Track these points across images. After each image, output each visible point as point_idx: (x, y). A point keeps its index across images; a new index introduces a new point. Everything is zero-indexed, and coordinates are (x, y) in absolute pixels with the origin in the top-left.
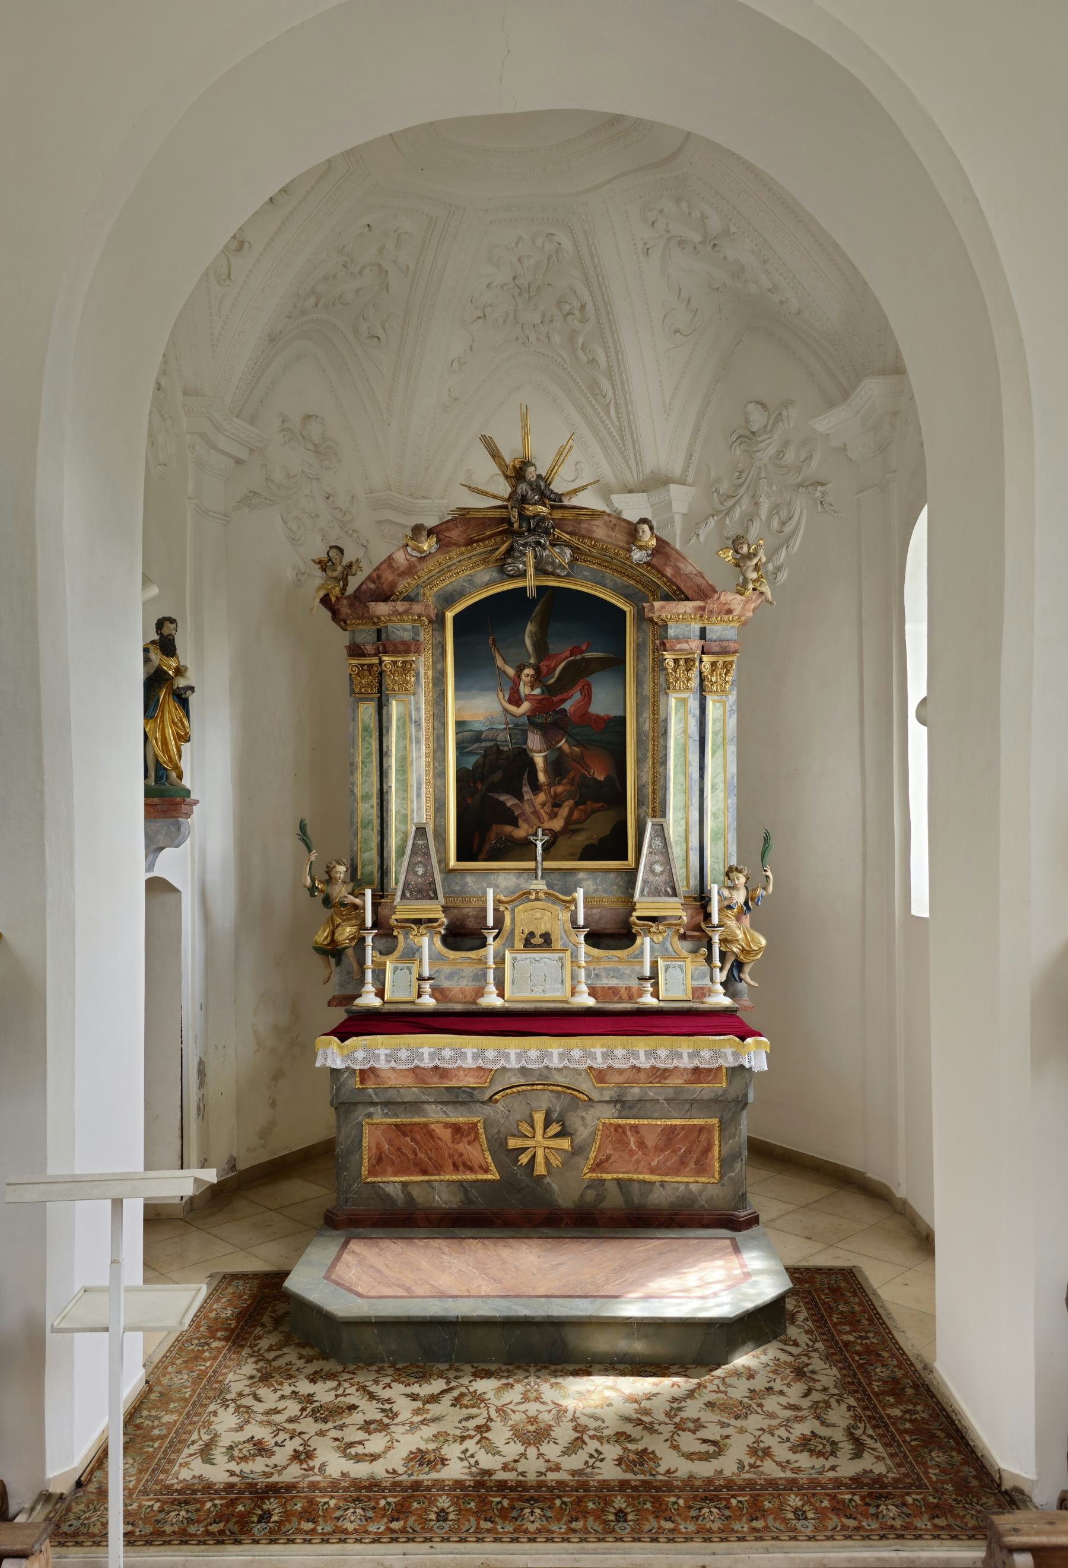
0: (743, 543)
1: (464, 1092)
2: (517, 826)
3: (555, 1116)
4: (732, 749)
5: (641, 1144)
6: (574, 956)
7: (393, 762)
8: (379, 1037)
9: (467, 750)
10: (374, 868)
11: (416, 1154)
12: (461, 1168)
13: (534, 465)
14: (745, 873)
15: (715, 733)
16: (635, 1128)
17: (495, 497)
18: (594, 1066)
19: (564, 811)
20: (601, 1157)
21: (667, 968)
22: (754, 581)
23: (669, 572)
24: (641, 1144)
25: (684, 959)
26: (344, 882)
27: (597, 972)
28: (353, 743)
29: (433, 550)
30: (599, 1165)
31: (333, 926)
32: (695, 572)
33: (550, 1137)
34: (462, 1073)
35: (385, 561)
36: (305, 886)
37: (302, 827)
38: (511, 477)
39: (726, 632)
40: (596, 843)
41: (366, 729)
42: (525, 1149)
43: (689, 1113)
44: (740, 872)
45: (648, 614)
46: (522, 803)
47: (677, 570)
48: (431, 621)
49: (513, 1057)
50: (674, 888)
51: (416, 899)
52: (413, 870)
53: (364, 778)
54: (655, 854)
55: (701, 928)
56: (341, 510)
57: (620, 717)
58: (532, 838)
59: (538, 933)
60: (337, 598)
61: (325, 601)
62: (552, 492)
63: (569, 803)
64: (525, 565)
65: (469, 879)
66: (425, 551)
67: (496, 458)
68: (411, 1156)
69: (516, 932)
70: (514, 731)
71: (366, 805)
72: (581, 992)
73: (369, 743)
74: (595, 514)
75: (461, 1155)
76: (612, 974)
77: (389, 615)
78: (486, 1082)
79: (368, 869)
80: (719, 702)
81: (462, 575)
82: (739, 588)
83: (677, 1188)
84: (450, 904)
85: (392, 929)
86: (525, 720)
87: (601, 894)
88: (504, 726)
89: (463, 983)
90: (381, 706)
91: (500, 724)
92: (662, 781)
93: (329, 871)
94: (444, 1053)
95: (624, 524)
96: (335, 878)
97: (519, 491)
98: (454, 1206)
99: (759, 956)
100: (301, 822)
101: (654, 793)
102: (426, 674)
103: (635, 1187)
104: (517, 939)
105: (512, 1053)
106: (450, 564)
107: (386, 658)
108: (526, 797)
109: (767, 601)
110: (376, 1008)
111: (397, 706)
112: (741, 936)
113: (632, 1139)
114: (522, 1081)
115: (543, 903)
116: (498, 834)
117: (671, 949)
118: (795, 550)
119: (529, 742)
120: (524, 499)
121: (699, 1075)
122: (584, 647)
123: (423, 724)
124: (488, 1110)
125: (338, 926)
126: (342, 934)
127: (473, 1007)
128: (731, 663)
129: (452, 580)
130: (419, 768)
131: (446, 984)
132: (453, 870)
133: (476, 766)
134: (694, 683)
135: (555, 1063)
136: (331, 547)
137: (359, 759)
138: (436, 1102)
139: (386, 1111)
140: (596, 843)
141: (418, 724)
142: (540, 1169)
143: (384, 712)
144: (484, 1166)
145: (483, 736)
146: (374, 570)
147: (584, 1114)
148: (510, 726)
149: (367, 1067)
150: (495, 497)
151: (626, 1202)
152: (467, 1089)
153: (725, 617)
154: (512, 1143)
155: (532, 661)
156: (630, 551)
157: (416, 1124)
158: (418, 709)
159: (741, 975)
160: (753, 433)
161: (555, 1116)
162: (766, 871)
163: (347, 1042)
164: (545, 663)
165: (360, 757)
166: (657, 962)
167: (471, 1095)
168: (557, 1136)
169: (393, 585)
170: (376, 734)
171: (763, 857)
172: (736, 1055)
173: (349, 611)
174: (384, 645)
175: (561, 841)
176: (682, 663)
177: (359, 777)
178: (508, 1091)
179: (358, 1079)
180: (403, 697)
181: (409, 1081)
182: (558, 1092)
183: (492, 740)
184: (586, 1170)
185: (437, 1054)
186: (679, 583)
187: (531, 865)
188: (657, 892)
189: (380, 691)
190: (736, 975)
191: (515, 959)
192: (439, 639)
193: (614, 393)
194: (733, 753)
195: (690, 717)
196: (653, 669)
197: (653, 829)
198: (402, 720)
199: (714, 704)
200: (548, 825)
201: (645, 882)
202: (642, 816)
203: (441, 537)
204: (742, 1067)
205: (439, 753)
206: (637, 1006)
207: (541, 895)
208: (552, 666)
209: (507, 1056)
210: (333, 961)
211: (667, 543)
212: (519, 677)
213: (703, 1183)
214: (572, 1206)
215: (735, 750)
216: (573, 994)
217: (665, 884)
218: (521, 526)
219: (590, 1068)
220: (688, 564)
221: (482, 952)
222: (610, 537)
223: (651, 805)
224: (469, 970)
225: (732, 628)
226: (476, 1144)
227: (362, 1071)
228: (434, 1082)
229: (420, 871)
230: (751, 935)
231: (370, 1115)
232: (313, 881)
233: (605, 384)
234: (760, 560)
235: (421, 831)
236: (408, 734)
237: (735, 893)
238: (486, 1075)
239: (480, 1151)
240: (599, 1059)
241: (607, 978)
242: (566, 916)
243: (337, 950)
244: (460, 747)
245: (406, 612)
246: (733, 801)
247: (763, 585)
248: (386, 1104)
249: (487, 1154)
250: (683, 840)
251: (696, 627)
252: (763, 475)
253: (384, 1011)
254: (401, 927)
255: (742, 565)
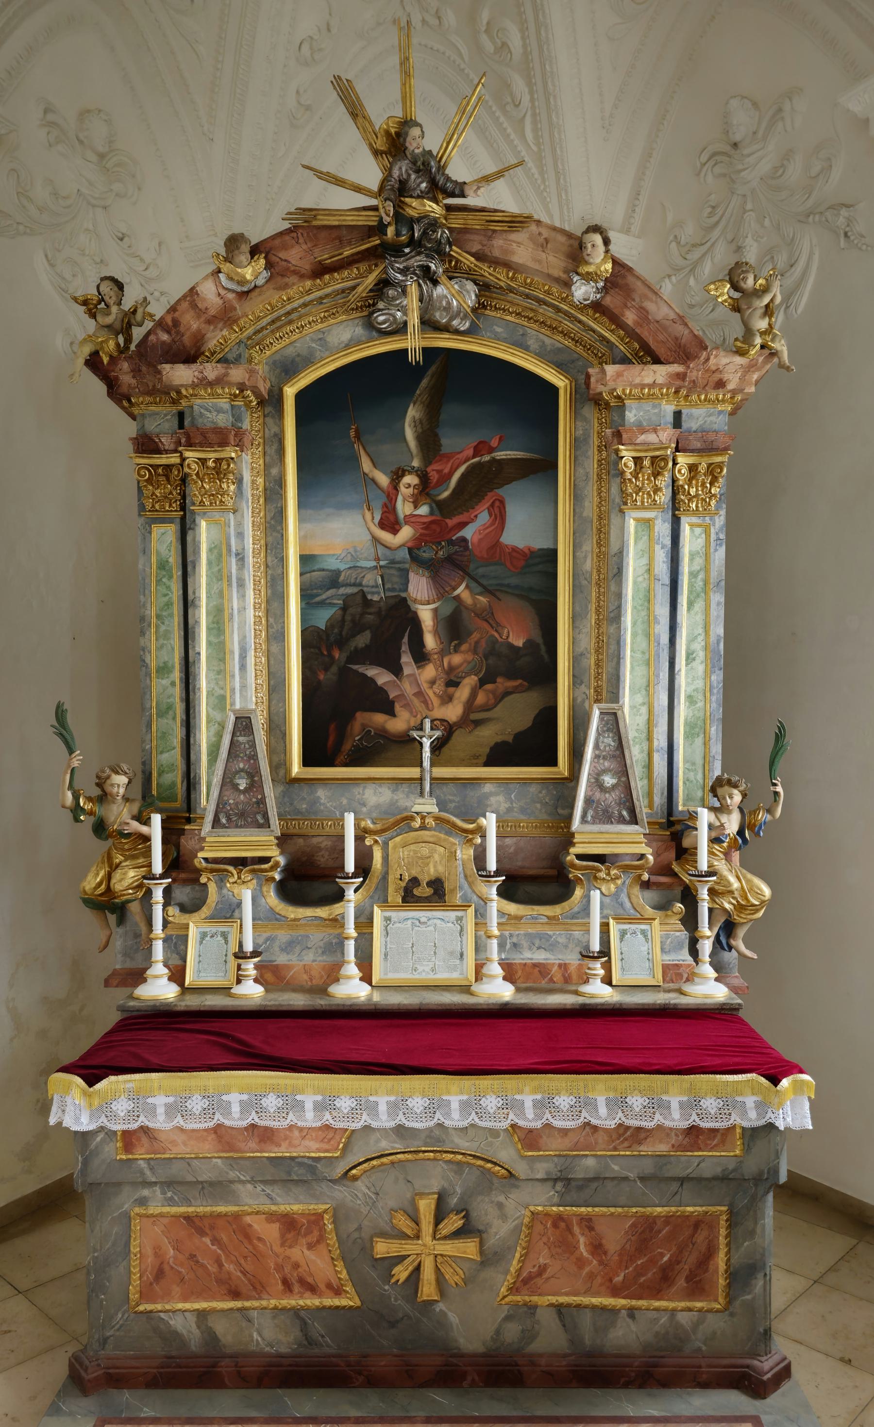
0: (747, 272)
1: (301, 1164)
2: (391, 713)
3: (453, 1201)
4: (718, 598)
5: (597, 1248)
6: (481, 915)
7: (202, 616)
8: (154, 1075)
9: (318, 599)
10: (177, 777)
11: (221, 1266)
12: (296, 1288)
13: (420, 126)
14: (742, 788)
15: (693, 575)
16: (588, 1223)
17: (358, 189)
18: (521, 1123)
19: (463, 693)
20: (529, 1269)
21: (623, 934)
22: (763, 333)
23: (630, 317)
24: (597, 1248)
25: (643, 919)
26: (126, 799)
27: (515, 940)
28: (144, 588)
29: (261, 281)
30: (525, 1282)
31: (110, 866)
32: (672, 316)
33: (445, 1238)
34: (296, 1133)
35: (184, 297)
36: (64, 807)
37: (60, 714)
38: (382, 153)
39: (713, 418)
40: (510, 741)
41: (163, 565)
42: (401, 1259)
43: (677, 1198)
44: (735, 786)
45: (596, 387)
46: (400, 680)
47: (643, 313)
48: (261, 403)
49: (383, 1108)
50: (632, 811)
51: (237, 827)
52: (231, 782)
53: (161, 641)
54: (604, 758)
55: (672, 870)
56: (142, 260)
57: (548, 550)
58: (415, 734)
59: (424, 879)
60: (111, 357)
61: (93, 362)
62: (448, 179)
63: (469, 683)
64: (405, 314)
65: (322, 793)
66: (248, 281)
67: (360, 119)
68: (213, 1268)
69: (391, 878)
70: (388, 571)
71: (165, 682)
72: (492, 977)
73: (168, 588)
74: (516, 222)
75: (296, 1266)
76: (537, 942)
77: (194, 386)
78: (337, 1149)
79: (168, 778)
80: (699, 526)
81: (307, 330)
82: (739, 344)
83: (656, 1320)
84: (292, 831)
85: (198, 872)
86: (404, 554)
87: (516, 815)
88: (374, 563)
89: (309, 957)
90: (185, 529)
91: (367, 559)
92: (613, 647)
93: (101, 783)
94: (265, 1102)
95: (562, 239)
96: (111, 795)
97: (396, 173)
98: (284, 1350)
99: (760, 914)
100: (58, 707)
101: (598, 665)
102: (253, 482)
103: (586, 1321)
104: (391, 889)
105: (383, 1102)
106: (289, 308)
107: (191, 455)
108: (407, 671)
109: (781, 366)
110: (168, 1004)
111: (208, 529)
112: (736, 885)
113: (582, 1240)
114: (399, 1147)
115: (433, 833)
116: (364, 726)
117: (628, 905)
118: (799, 311)
119: (411, 588)
120: (403, 189)
121: (697, 1137)
122: (494, 443)
123: (250, 560)
124: (341, 1193)
125: (118, 866)
126: (121, 880)
127: (320, 1002)
128: (720, 466)
129: (293, 338)
130: (242, 624)
131: (281, 959)
132: (297, 780)
133: (331, 624)
134: (664, 497)
135: (455, 1119)
136: (103, 279)
137: (152, 612)
138: (253, 1181)
139: (169, 1194)
140: (510, 741)
141: (241, 558)
142: (428, 1290)
143: (189, 538)
144: (335, 1282)
145: (342, 578)
146: (168, 312)
147: (501, 1198)
148: (382, 563)
149: (134, 1126)
150: (358, 189)
151: (572, 1342)
152: (306, 1161)
153: (712, 396)
154: (382, 1248)
155: (416, 463)
156: (568, 284)
157: (220, 1216)
158: (240, 535)
159: (733, 942)
160: (735, 145)
161: (453, 1201)
162: (775, 785)
163: (98, 1086)
164: (436, 466)
165: (154, 609)
166: (608, 924)
167: (312, 1170)
168: (458, 1234)
169: (199, 339)
170: (177, 573)
171: (772, 763)
172: (761, 1106)
173: (133, 382)
174: (188, 437)
175: (459, 737)
176: (647, 463)
177: (153, 638)
178: (374, 1162)
179: (119, 1144)
180: (217, 516)
181: (207, 1148)
182: (459, 1163)
183: (354, 585)
184: (503, 1290)
185: (252, 1105)
186: (645, 334)
187: (413, 772)
188: (606, 817)
189: (183, 508)
190: (724, 941)
191: (388, 919)
192: (275, 429)
193: (532, 100)
194: (719, 604)
195: (657, 548)
196: (600, 478)
197: (601, 719)
198: (216, 551)
199: (692, 530)
200: (441, 712)
201: (588, 801)
202: (579, 700)
203: (273, 259)
204: (771, 1127)
205: (275, 604)
206: (580, 1000)
207: (430, 821)
208: (446, 471)
209: (373, 1108)
210: (112, 918)
211: (630, 269)
212: (396, 488)
213: (700, 1310)
214: (481, 1349)
215: (723, 600)
216: (479, 977)
217: (619, 804)
218: (398, 234)
219: (514, 1126)
220: (662, 304)
221: (336, 909)
222: (539, 262)
223: (593, 684)
224: (318, 937)
225: (720, 412)
226: (322, 1247)
227: (125, 1133)
228: (252, 1150)
229: (243, 784)
230: (748, 881)
231: (142, 1202)
232: (76, 798)
233: (519, 85)
234: (772, 300)
235: (244, 724)
236: (225, 572)
237: (724, 818)
238: (337, 1137)
239: (328, 1259)
240: (530, 1113)
241: (530, 949)
242: (464, 854)
243: (113, 904)
244: (307, 595)
245: (219, 381)
246: (717, 678)
247: (777, 340)
248: (169, 1184)
249: (340, 1266)
250: (644, 735)
251: (668, 409)
252: (749, 206)
253: (179, 1009)
254: (212, 871)
255: (744, 307)
